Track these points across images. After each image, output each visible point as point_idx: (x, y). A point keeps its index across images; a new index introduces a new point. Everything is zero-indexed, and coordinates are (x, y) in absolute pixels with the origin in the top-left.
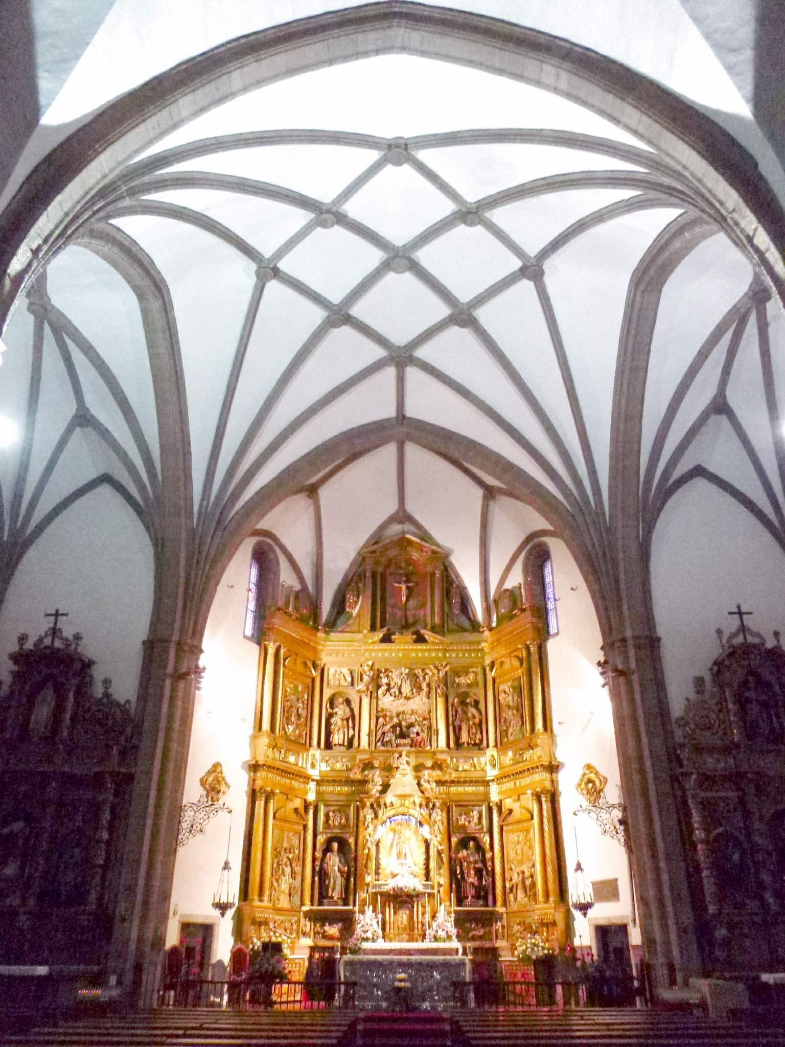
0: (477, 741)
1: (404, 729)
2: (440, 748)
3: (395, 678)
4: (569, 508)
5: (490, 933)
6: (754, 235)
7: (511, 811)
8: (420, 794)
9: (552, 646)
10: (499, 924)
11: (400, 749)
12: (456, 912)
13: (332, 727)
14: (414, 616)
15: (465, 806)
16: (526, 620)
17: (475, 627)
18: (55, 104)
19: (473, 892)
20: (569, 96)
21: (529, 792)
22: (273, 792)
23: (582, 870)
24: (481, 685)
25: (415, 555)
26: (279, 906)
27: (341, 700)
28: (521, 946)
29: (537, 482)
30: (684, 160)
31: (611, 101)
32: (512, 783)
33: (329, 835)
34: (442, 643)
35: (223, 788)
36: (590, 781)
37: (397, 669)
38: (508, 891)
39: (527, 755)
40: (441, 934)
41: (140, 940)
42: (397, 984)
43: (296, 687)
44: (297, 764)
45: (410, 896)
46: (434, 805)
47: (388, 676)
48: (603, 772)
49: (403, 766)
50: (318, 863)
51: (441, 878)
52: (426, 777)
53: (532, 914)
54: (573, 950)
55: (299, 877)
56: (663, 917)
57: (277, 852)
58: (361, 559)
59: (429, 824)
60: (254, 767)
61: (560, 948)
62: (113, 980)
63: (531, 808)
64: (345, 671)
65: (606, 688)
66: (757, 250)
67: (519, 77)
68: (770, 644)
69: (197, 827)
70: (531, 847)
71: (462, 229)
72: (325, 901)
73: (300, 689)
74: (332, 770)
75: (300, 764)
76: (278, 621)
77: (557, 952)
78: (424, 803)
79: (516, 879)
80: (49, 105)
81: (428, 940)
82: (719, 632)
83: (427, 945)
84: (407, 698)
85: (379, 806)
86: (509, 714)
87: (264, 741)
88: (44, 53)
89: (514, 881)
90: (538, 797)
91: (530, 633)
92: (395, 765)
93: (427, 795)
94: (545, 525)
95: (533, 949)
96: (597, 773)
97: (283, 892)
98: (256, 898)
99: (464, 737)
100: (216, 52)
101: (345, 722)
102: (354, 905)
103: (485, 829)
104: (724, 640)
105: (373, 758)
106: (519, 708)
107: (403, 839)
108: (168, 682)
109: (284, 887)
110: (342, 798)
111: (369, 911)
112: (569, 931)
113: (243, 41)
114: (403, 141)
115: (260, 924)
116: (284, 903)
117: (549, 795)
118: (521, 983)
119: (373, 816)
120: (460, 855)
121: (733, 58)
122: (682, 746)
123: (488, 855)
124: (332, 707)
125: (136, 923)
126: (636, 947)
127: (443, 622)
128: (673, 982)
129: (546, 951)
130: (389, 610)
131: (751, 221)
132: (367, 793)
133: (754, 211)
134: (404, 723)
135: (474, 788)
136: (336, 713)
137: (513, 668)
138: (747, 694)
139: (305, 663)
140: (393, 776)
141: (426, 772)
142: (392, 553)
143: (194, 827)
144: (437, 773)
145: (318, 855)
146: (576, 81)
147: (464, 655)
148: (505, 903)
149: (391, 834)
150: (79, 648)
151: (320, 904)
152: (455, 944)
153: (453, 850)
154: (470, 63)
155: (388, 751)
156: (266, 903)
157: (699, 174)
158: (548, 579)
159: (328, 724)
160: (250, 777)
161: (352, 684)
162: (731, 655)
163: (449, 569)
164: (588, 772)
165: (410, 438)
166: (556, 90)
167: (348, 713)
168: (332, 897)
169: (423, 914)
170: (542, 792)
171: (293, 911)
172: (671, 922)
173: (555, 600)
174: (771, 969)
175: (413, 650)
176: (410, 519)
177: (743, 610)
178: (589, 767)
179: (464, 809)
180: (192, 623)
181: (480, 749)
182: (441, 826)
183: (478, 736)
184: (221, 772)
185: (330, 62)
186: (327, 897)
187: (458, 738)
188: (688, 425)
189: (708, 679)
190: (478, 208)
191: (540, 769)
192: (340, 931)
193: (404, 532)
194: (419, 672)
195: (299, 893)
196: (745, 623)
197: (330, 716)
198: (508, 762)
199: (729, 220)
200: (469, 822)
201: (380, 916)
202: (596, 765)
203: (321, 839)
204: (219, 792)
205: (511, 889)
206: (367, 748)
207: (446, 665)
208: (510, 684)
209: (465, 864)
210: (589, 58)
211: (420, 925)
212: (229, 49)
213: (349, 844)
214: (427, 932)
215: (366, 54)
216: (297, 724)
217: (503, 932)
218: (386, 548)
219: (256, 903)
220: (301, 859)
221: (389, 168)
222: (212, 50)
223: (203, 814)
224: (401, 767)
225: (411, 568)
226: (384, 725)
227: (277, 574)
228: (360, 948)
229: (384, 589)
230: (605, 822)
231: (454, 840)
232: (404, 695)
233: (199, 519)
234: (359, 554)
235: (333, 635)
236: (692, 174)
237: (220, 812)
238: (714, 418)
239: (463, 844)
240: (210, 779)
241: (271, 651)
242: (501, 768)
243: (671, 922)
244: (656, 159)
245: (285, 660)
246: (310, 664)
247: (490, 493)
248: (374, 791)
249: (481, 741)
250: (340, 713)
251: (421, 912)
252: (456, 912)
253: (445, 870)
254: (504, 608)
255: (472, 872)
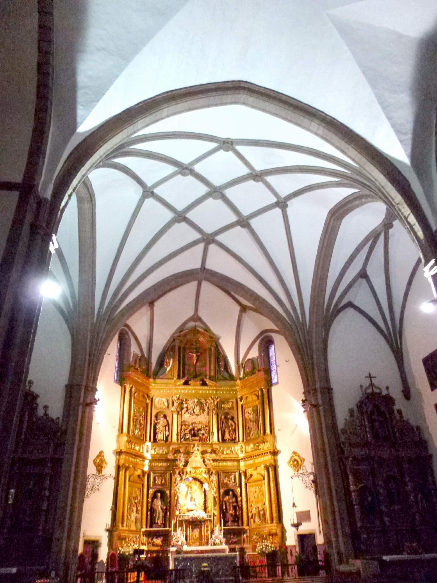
0: (233, 439)
1: (196, 432)
2: (214, 442)
3: (190, 404)
4: (289, 321)
5: (241, 539)
6: (408, 217)
7: (251, 475)
8: (205, 466)
9: (274, 390)
10: (245, 535)
11: (194, 442)
12: (224, 529)
13: (157, 430)
14: (199, 371)
15: (228, 474)
16: (261, 375)
17: (232, 378)
18: (85, 122)
19: (232, 518)
20: (322, 137)
21: (263, 466)
22: (129, 467)
23: (295, 506)
24: (235, 408)
25: (201, 339)
26: (131, 529)
27: (162, 416)
28: (260, 546)
29: (271, 306)
30: (376, 177)
31: (343, 144)
32: (253, 461)
33: (156, 489)
34: (215, 386)
35: (104, 465)
36: (295, 460)
37: (191, 399)
38: (250, 517)
39: (261, 446)
40: (217, 541)
41: (67, 550)
42: (202, 569)
43: (139, 408)
44: (140, 451)
45: (200, 522)
46: (212, 473)
47: (187, 403)
48: (302, 456)
49: (196, 452)
50: (149, 505)
51: (214, 511)
52: (208, 458)
53: (264, 529)
54: (286, 547)
55: (140, 513)
56: (336, 529)
57: (130, 501)
58: (173, 339)
59: (208, 483)
60: (119, 453)
61: (279, 546)
62: (53, 574)
63: (263, 475)
64: (164, 400)
65: (306, 412)
66: (409, 223)
67: (299, 125)
68: (384, 393)
69: (96, 487)
70: (263, 494)
71: (251, 182)
72: (154, 525)
73: (141, 410)
74: (157, 454)
75: (141, 451)
76: (132, 374)
77: (278, 548)
78: (207, 472)
79: (254, 511)
80: (82, 123)
81: (210, 545)
82: (361, 386)
83: (209, 547)
84: (197, 415)
85: (183, 473)
86: (251, 425)
87: (125, 439)
88: (81, 96)
89: (253, 512)
90: (267, 468)
91: (263, 383)
92: (191, 451)
93: (208, 467)
94: (273, 327)
95: (266, 548)
96: (299, 456)
97: (133, 521)
98: (120, 525)
99: (227, 436)
100: (156, 98)
101: (164, 428)
102: (170, 526)
103: (238, 485)
104: (363, 390)
105: (180, 447)
106: (257, 421)
107: (193, 490)
108: (80, 408)
109: (133, 518)
110: (162, 469)
111: (179, 530)
112: (283, 538)
113: (170, 93)
114: (231, 140)
115: (122, 539)
116: (133, 528)
117: (273, 467)
118: (259, 566)
119: (180, 479)
120: (225, 499)
121: (403, 137)
122: (344, 443)
123: (239, 499)
124: (157, 420)
125: (65, 542)
126: (320, 545)
127: (216, 374)
128: (341, 562)
129: (273, 549)
130: (187, 367)
131: (408, 211)
132: (177, 466)
133: (409, 206)
134: (196, 429)
135: (232, 463)
136: (159, 423)
137: (253, 400)
138: (373, 417)
139: (143, 396)
140: (190, 457)
141: (208, 455)
142: (188, 337)
143: (94, 487)
144: (213, 456)
145: (150, 500)
146: (326, 132)
147: (226, 392)
148: (248, 525)
149: (186, 488)
150: (31, 388)
151: (151, 527)
152: (226, 547)
153: (221, 496)
154: (276, 115)
155: (187, 444)
156: (125, 528)
157: (383, 184)
158: (272, 354)
159: (155, 429)
160: (116, 458)
161: (168, 407)
162: (367, 398)
163: (219, 347)
164: (294, 455)
165: (207, 280)
166: (316, 134)
167: (166, 423)
168: (157, 523)
169: (207, 531)
170: (270, 466)
171: (137, 531)
172: (340, 532)
173: (277, 366)
174: (387, 554)
175: (200, 390)
176: (200, 320)
177: (372, 375)
178: (295, 453)
179: (227, 474)
180: (93, 375)
181: (235, 443)
182: (215, 483)
183: (234, 436)
184: (103, 456)
185: (209, 106)
186: (155, 523)
187: (223, 436)
188: (348, 282)
189: (355, 409)
190: (261, 174)
191: (269, 454)
192: (162, 541)
193: (196, 326)
194: (203, 401)
195: (140, 521)
196: (373, 382)
197: (155, 424)
198: (250, 450)
199: (396, 207)
200: (229, 481)
201: (185, 533)
202: (298, 452)
203: (151, 491)
204: (102, 467)
205: (252, 516)
206: (176, 442)
207: (217, 399)
208: (251, 408)
209: (228, 504)
210: (333, 122)
211: (205, 537)
212: (163, 97)
213: (167, 494)
214: (209, 541)
215: (226, 104)
216: (140, 429)
217: (247, 539)
218: (185, 335)
219: (121, 528)
220: (141, 502)
221: (222, 152)
222: (154, 97)
223: (99, 480)
224: (195, 452)
225: (198, 345)
226: (185, 430)
227: (129, 346)
228: (182, 551)
229: (184, 356)
230: (306, 482)
231: (222, 491)
232: (196, 413)
233: (97, 319)
234: (172, 336)
235: (158, 381)
236: (379, 183)
237: (109, 479)
238: (360, 280)
239: (226, 493)
240: (98, 461)
241: (128, 389)
242: (246, 452)
243: (340, 532)
244: (358, 169)
245: (134, 394)
246: (146, 396)
247: (244, 309)
248: (181, 465)
249: (235, 438)
250: (161, 423)
251: (206, 531)
252: (224, 529)
253: (217, 507)
254: (249, 368)
255: (232, 508)
